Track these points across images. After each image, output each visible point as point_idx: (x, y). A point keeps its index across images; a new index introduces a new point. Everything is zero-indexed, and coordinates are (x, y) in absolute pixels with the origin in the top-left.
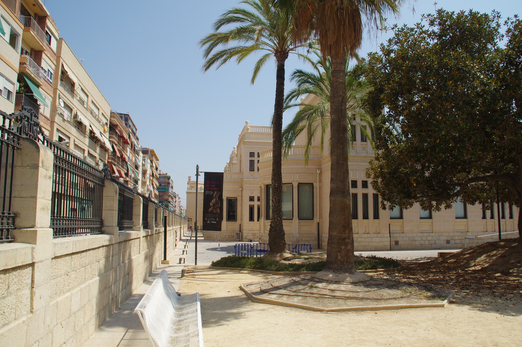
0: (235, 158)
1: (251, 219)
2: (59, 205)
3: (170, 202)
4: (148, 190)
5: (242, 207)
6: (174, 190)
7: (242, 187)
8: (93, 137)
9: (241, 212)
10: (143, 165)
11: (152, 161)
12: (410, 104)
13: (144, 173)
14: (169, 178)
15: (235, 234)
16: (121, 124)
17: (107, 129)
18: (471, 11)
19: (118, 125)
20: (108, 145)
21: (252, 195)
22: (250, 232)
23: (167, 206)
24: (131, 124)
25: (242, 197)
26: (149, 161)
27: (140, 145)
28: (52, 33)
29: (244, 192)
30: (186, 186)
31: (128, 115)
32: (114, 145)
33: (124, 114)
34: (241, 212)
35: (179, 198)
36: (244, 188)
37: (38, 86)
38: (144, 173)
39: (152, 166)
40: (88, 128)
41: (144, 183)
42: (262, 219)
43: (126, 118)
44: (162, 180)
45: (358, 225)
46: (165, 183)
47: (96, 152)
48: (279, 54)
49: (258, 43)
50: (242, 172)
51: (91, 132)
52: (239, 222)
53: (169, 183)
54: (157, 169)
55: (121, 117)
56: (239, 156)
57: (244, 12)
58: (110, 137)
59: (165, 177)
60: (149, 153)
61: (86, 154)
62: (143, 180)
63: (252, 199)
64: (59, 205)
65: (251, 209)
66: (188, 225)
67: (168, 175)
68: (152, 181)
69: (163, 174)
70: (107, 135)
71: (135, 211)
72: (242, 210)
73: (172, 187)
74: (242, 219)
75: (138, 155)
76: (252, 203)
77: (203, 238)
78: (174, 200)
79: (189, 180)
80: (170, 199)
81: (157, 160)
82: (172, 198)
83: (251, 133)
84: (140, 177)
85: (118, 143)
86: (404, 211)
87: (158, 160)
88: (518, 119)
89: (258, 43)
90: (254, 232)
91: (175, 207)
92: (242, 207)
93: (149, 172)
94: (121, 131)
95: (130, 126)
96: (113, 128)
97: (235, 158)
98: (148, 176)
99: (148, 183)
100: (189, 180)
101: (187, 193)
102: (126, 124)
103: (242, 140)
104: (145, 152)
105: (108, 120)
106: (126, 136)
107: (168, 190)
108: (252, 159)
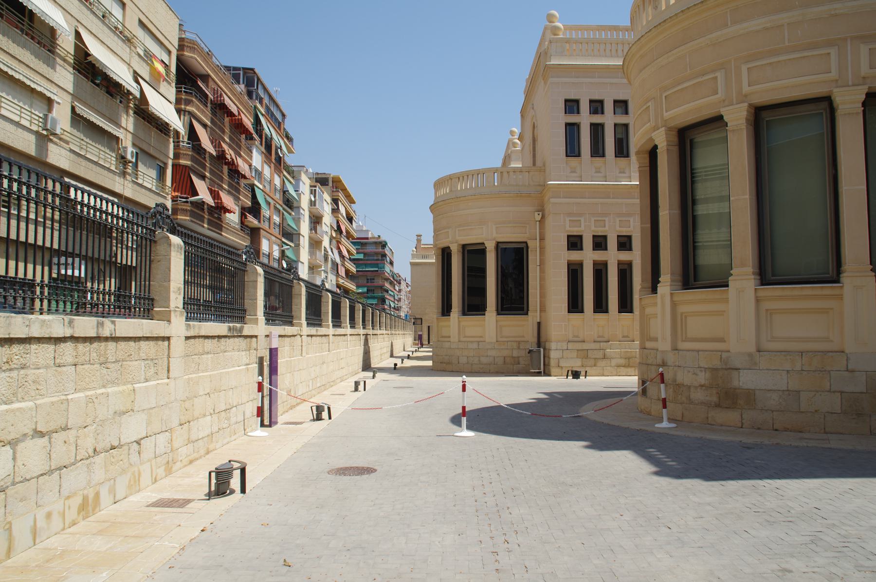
1: (575, 305)
3: (387, 291)
4: (326, 258)
5: (542, 271)
6: (396, 269)
7: (541, 210)
9: (542, 287)
10: (312, 203)
11: (335, 201)
13: (316, 220)
14: (384, 245)
15: (523, 353)
18: (464, 408)
19: (209, 76)
20: (176, 123)
21: (575, 231)
22: (571, 346)
23: (383, 300)
25: (542, 239)
29: (549, 222)
31: (252, 70)
32: (195, 123)
33: (244, 69)
34: (542, 287)
36: (548, 208)
39: (335, 211)
40: (66, 44)
41: (315, 244)
42: (664, 288)
44: (370, 249)
46: (377, 254)
47: (119, 125)
50: (539, 163)
51: (348, 232)
52: (534, 316)
53: (384, 255)
54: (350, 219)
55: (236, 78)
58: (178, 101)
59: (376, 243)
60: (330, 184)
61: (61, 116)
62: (314, 235)
63: (575, 243)
65: (574, 273)
66: (415, 331)
67: (383, 238)
68: (339, 242)
69: (374, 238)
71: (342, 313)
72: (542, 279)
73: (391, 263)
74: (543, 309)
76: (575, 256)
77: (429, 363)
78: (397, 288)
79: (419, 241)
80: (387, 285)
82: (391, 283)
83: (568, 41)
84: (305, 228)
85: (212, 122)
87: (354, 202)
90: (585, 346)
91: (399, 300)
92: (542, 271)
93: (328, 219)
99: (326, 243)
100: (419, 241)
101: (412, 264)
102: (250, 94)
103: (541, 71)
105: (169, 53)
106: (248, 122)
107: (384, 267)
108: (572, 119)
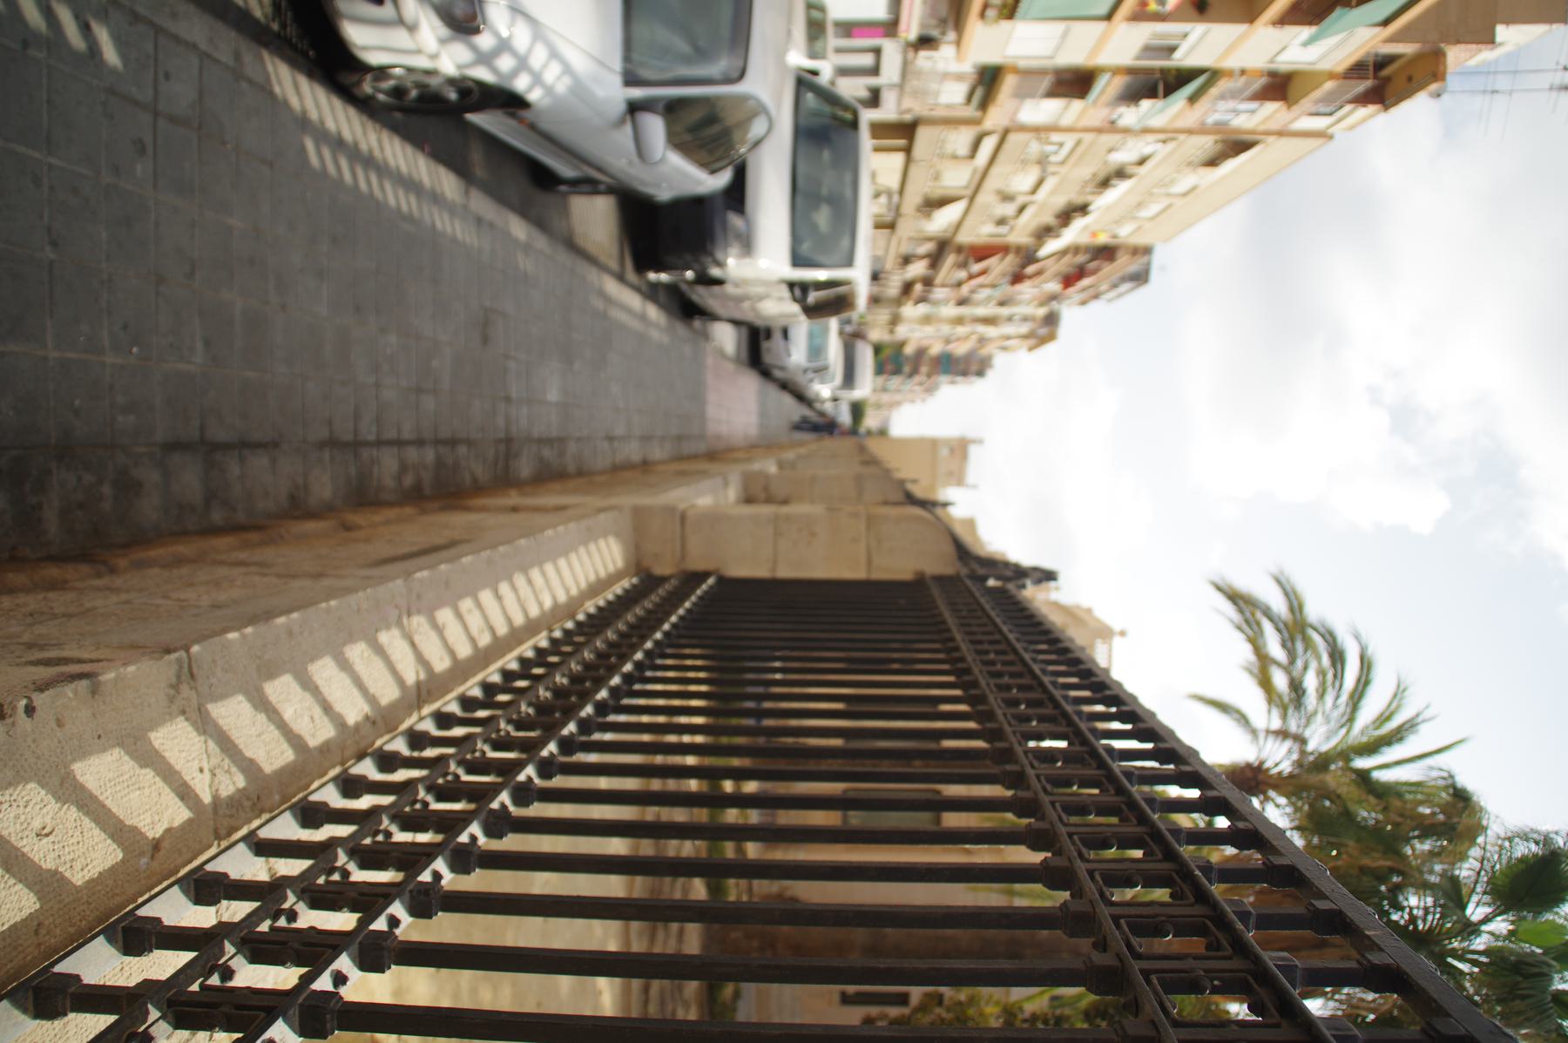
2: (885, 767)
12: (37, 991)
13: (989, 321)
16: (1124, 264)
17: (1103, 239)
27: (1071, 315)
28: (1340, 120)
37: (1193, 99)
38: (989, 321)
43: (1141, 278)
48: (1249, 774)
49: (1262, 736)
57: (1364, 682)
64: (885, 767)
75: (1042, 304)
84: (981, 311)
86: (102, 937)
89: (1262, 736)
94: (1094, 272)
96: (1106, 253)
104: (1051, 320)
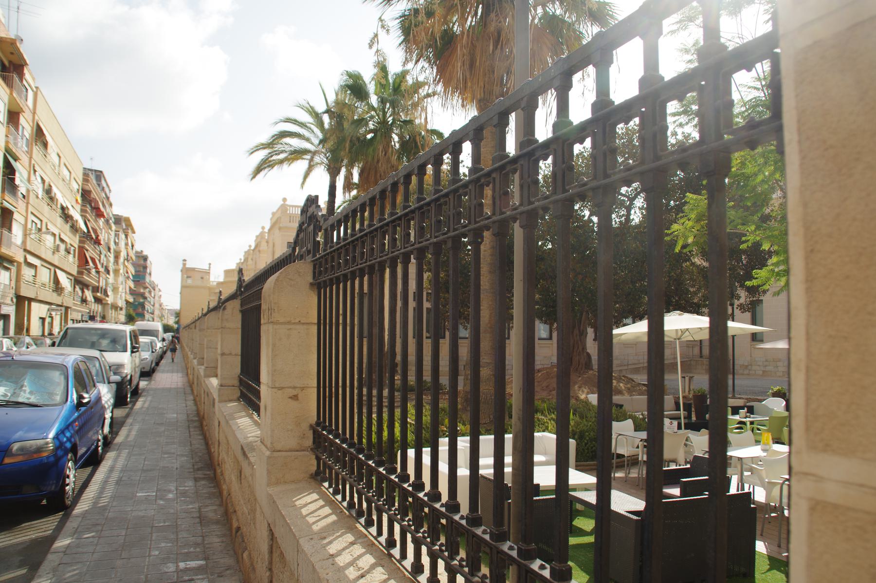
0: (264, 244)
8: (66, 216)
11: (126, 236)
13: (117, 257)
16: (92, 186)
24: (104, 184)
26: (123, 236)
30: (178, 276)
31: (101, 172)
35: (160, 290)
38: (117, 257)
45: (351, 568)
56: (271, 245)
58: (82, 211)
67: (145, 253)
70: (78, 207)
73: (150, 274)
79: (184, 265)
80: (147, 295)
81: (134, 232)
88: (594, 231)
93: (123, 254)
95: (103, 189)
97: (264, 244)
98: (121, 260)
100: (184, 265)
104: (118, 220)
107: (144, 279)
